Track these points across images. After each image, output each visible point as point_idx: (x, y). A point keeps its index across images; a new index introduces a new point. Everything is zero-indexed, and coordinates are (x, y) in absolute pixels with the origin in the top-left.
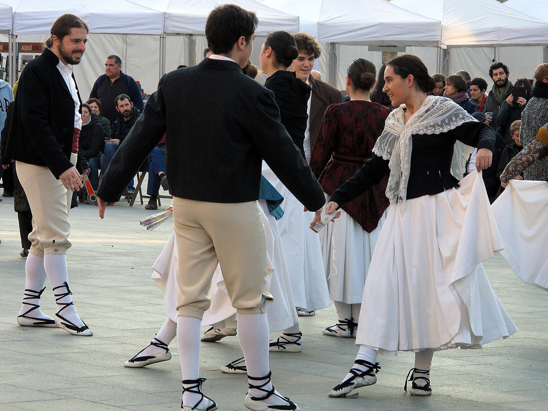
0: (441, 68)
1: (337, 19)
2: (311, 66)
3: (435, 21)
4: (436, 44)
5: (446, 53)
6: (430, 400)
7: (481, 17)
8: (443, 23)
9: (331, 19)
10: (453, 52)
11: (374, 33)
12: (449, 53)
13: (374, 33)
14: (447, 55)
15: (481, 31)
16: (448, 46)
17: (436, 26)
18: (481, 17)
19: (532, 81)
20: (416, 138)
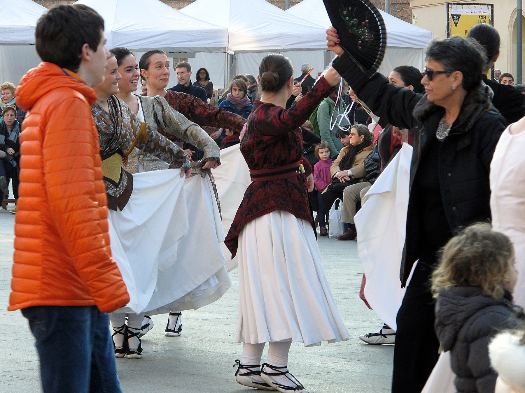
0: (229, 73)
1: (131, 27)
2: (211, 85)
3: (223, 28)
4: (223, 50)
5: (233, 58)
6: (181, 339)
7: (265, 25)
8: (230, 30)
9: (125, 28)
10: (240, 56)
11: (165, 40)
12: (235, 58)
13: (165, 40)
14: (234, 60)
15: (265, 37)
16: (234, 52)
17: (216, 34)
18: (265, 25)
19: (314, 81)
20: (341, 169)
